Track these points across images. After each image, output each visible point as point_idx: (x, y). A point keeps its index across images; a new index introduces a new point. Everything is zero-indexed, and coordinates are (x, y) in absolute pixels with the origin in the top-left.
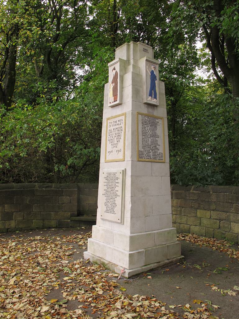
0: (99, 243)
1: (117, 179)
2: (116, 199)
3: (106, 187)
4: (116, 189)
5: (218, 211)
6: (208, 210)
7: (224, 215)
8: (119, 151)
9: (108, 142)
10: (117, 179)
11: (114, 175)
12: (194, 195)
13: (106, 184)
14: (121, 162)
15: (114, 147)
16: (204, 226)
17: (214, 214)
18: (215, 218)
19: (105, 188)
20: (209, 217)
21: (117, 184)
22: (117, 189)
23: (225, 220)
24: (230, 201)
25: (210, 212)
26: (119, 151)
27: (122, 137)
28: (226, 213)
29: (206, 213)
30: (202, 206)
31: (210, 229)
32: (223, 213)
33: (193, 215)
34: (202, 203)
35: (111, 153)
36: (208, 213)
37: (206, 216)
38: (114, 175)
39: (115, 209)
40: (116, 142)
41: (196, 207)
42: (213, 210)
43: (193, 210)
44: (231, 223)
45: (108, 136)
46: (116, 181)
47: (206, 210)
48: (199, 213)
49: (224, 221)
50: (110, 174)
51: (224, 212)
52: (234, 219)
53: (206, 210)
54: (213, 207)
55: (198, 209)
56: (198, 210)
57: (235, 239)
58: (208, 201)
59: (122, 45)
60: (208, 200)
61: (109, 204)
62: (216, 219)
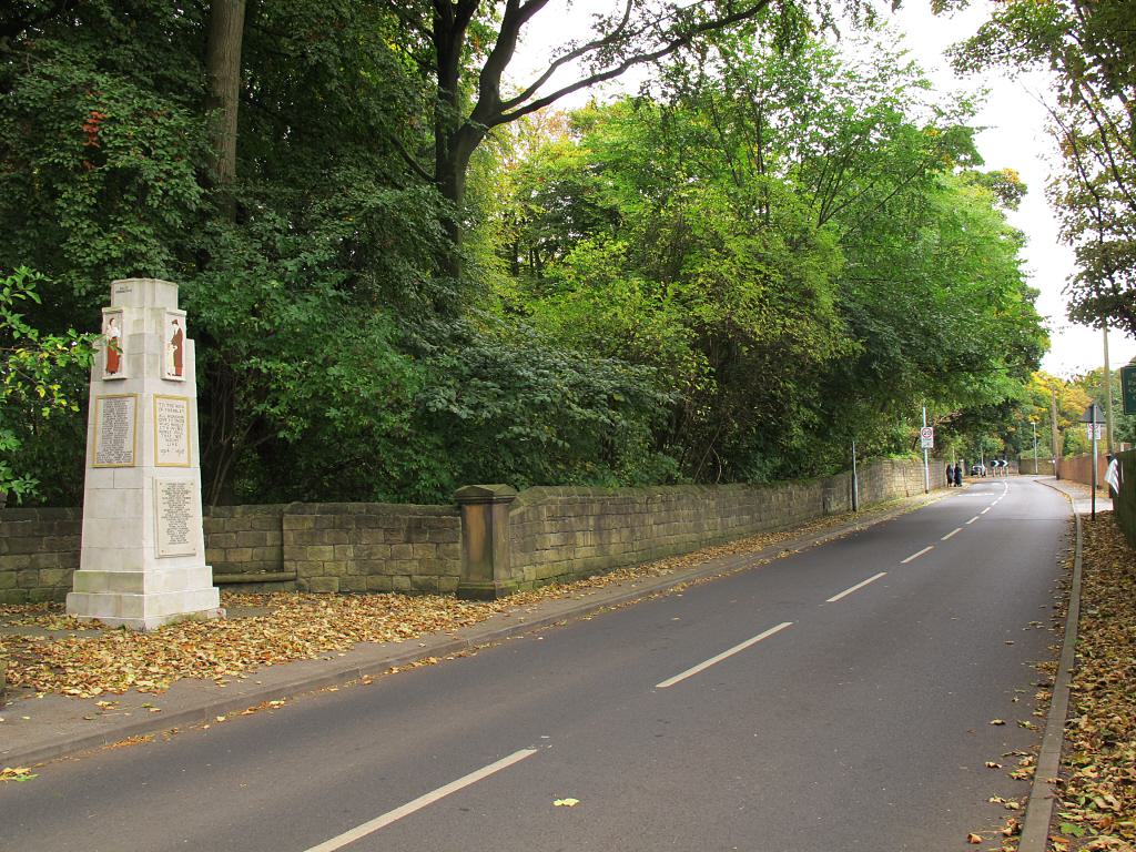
7: (26, 560)
24: (36, 534)
40: (173, 437)
49: (25, 571)
51: (24, 554)
52: (47, 562)
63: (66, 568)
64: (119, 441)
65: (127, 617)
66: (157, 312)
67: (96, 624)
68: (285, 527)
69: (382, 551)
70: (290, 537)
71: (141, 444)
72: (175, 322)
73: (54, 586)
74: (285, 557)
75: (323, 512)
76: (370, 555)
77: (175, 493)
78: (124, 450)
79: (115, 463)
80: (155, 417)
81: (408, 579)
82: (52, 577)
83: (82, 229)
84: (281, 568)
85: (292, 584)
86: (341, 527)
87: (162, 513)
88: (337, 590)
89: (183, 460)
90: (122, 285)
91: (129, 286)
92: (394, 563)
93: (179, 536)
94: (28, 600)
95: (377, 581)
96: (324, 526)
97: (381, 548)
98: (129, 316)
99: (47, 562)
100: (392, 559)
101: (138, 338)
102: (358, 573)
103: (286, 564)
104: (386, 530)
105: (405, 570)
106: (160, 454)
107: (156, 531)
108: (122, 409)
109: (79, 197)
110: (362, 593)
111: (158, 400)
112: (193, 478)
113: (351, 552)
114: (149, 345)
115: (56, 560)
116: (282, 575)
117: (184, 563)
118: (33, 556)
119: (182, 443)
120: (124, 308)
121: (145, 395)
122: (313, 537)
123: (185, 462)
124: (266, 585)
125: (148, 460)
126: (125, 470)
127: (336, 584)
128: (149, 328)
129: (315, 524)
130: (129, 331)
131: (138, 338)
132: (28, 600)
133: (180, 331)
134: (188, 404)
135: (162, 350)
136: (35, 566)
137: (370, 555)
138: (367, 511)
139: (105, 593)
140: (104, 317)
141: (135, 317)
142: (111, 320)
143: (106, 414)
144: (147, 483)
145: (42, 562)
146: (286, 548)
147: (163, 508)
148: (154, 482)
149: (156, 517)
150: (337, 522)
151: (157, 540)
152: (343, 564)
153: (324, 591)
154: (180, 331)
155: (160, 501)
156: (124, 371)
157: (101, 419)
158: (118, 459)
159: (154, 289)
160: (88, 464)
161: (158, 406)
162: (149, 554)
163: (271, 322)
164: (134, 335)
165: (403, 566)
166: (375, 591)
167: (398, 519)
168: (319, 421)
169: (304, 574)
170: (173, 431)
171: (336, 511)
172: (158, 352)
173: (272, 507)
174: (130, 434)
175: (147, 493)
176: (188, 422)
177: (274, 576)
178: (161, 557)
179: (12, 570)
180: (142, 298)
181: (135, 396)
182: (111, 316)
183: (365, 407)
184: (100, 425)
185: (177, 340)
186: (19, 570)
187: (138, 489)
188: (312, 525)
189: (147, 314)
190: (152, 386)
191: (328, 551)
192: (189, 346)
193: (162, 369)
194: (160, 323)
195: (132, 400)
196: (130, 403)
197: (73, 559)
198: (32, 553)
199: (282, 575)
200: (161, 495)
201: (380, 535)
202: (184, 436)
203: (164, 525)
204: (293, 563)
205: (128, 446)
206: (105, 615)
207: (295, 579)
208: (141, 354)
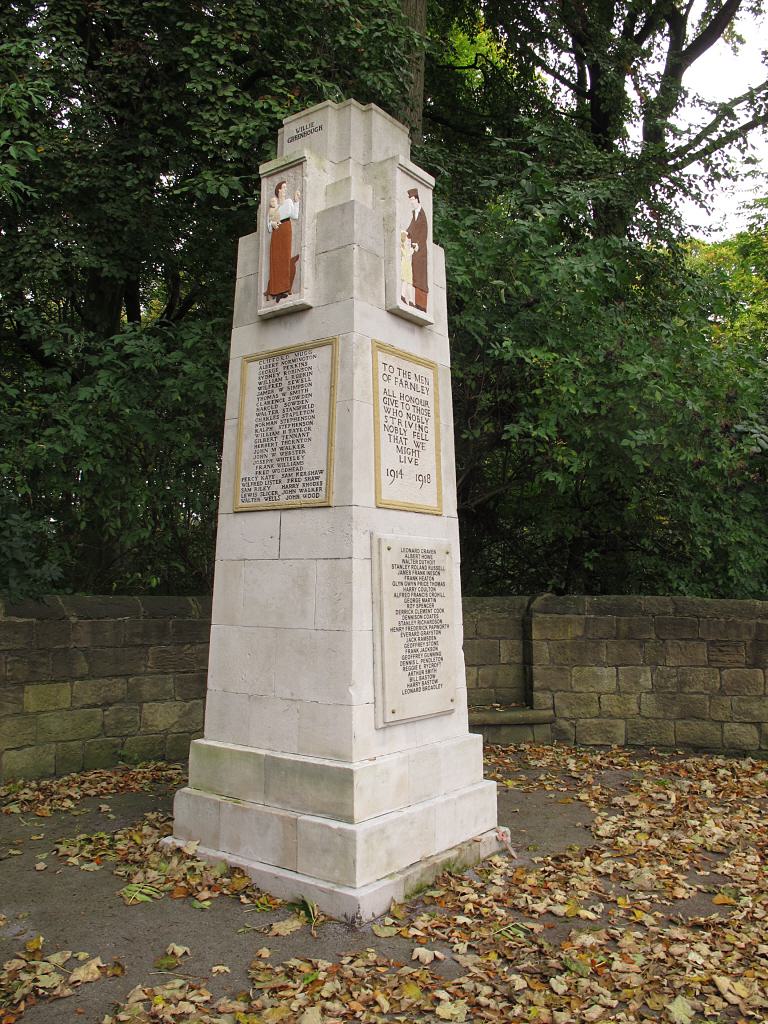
0: (401, 814)
1: (438, 570)
2: (438, 637)
3: (402, 599)
4: (437, 605)
5: (99, 678)
6: (65, 682)
7: (119, 687)
8: (423, 479)
9: (384, 435)
10: (438, 570)
11: (429, 557)
12: (16, 633)
13: (400, 589)
14: (431, 517)
15: (407, 461)
16: (50, 742)
17: (87, 691)
18: (89, 702)
19: (401, 603)
20: (67, 706)
21: (439, 589)
22: (439, 603)
23: (121, 701)
24: (138, 641)
25: (72, 686)
26: (423, 479)
27: (431, 436)
28: (123, 680)
29: (58, 691)
30: (42, 670)
31: (72, 744)
32: (114, 680)
33: (11, 708)
34: (43, 660)
35: (398, 480)
36: (64, 693)
37: (55, 704)
38: (429, 557)
39: (440, 672)
40: (411, 445)
41: (20, 677)
42: (82, 678)
43: (13, 692)
44: (145, 705)
45: (382, 413)
46: (437, 579)
47: (56, 682)
48: (31, 697)
49: (118, 706)
50: (412, 553)
51: (116, 676)
52: (155, 690)
53: (58, 682)
54: (82, 666)
55: (28, 682)
56: (27, 688)
57: (157, 748)
58: (66, 649)
59: (389, 116)
60: (63, 646)
61: (419, 660)
62: (89, 706)
63: (186, 701)
64: (292, 450)
65: (309, 880)
66: (375, 172)
67: (239, 883)
68: (535, 634)
69: (703, 679)
70: (542, 651)
71: (347, 460)
72: (413, 193)
73: (166, 732)
74: (536, 684)
75: (601, 611)
76: (682, 684)
77: (416, 566)
78: (307, 468)
79: (283, 500)
80: (376, 392)
81: (754, 730)
82: (162, 716)
83: (224, 98)
84: (528, 701)
85: (546, 730)
86: (630, 637)
87: (391, 620)
88: (622, 742)
89: (427, 497)
90: (303, 123)
91: (316, 120)
92: (726, 701)
93: (422, 679)
94: (123, 758)
95: (694, 729)
96: (600, 634)
97: (703, 673)
98: (318, 176)
99: (155, 690)
100: (722, 692)
101: (340, 213)
102: (660, 714)
103: (538, 696)
104: (712, 643)
105: (748, 713)
106: (385, 479)
107: (378, 664)
108: (300, 381)
109: (221, 43)
110: (670, 748)
111: (381, 357)
112: (443, 536)
113: (646, 679)
114: (364, 230)
115: (170, 686)
116: (530, 714)
117: (430, 733)
118: (131, 680)
119: (427, 462)
120: (306, 153)
121: (355, 337)
122: (582, 652)
123: (432, 503)
124: (504, 731)
125: (362, 493)
126: (309, 513)
127: (620, 730)
128: (360, 193)
129: (585, 631)
130: (317, 203)
131: (340, 213)
132: (123, 758)
133: (422, 213)
134: (435, 375)
135: (389, 244)
136: (135, 699)
137: (682, 684)
138: (676, 611)
139: (257, 804)
140: (264, 183)
141: (328, 179)
142: (279, 186)
143: (265, 392)
144: (360, 546)
145: (147, 689)
146: (537, 670)
147: (392, 605)
148: (376, 544)
149: (378, 630)
150: (624, 628)
151: (380, 685)
152: (633, 699)
153: (599, 743)
154: (422, 213)
155: (387, 587)
156: (308, 289)
157: (252, 402)
158: (289, 490)
159: (369, 127)
160: (225, 503)
161: (381, 370)
162: (362, 719)
163: (533, 283)
164: (336, 183)
165: (744, 706)
166: (698, 749)
167: (737, 626)
168: (609, 454)
169: (567, 714)
170: (410, 432)
171: (620, 611)
172: (381, 251)
173: (507, 601)
174: (318, 432)
175: (360, 570)
176: (437, 416)
177: (520, 715)
178: (388, 726)
179: (95, 706)
180: (345, 142)
181: (330, 342)
182: (277, 179)
183: (685, 431)
184: (250, 419)
185: (416, 231)
186: (107, 704)
187: (340, 559)
188: (580, 633)
189: (354, 172)
190: (369, 323)
191: (607, 677)
192: (437, 258)
193: (389, 288)
194: (386, 193)
195: (324, 354)
196: (319, 361)
197: (195, 684)
198: (131, 675)
199: (530, 714)
200: (391, 575)
201: (702, 652)
202: (430, 445)
203: (396, 646)
204: (549, 695)
205: (313, 458)
206: (260, 863)
207: (551, 722)
208: (346, 248)
